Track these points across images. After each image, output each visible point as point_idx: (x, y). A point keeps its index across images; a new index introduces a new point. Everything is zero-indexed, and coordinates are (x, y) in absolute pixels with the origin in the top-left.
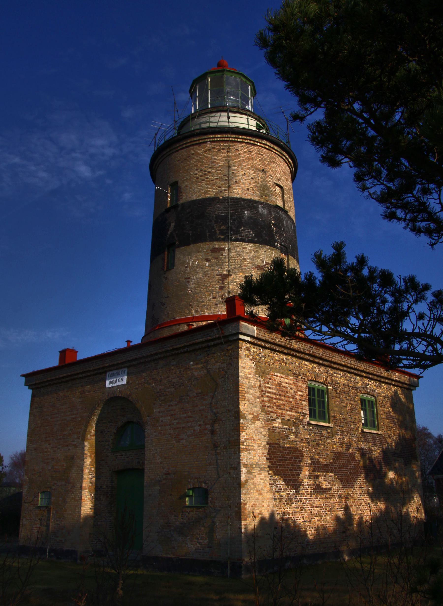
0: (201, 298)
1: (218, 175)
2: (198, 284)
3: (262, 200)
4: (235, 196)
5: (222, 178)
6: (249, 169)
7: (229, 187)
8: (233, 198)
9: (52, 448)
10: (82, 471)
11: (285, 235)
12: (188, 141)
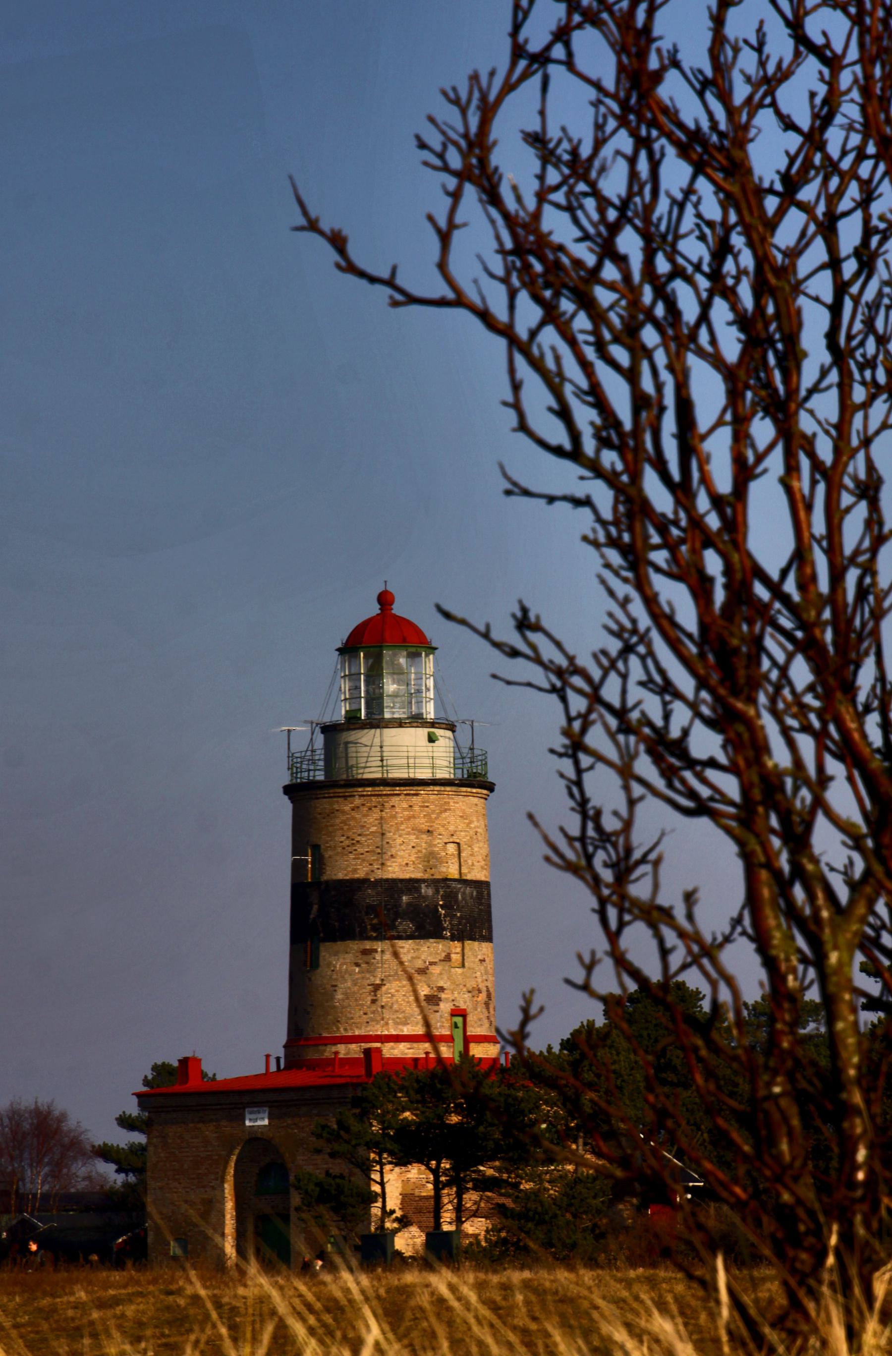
0: (350, 1013)
1: (368, 846)
2: (347, 996)
3: (426, 876)
4: (390, 876)
5: (373, 851)
6: (409, 833)
7: (383, 864)
8: (387, 880)
9: (184, 1188)
10: (224, 1216)
11: (459, 914)
12: (331, 791)
